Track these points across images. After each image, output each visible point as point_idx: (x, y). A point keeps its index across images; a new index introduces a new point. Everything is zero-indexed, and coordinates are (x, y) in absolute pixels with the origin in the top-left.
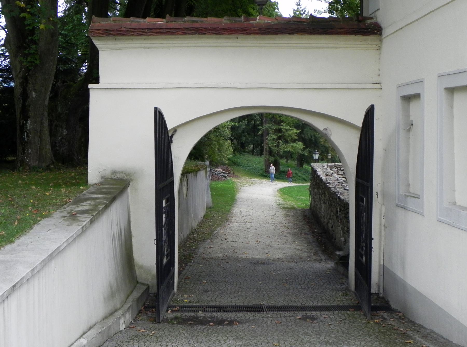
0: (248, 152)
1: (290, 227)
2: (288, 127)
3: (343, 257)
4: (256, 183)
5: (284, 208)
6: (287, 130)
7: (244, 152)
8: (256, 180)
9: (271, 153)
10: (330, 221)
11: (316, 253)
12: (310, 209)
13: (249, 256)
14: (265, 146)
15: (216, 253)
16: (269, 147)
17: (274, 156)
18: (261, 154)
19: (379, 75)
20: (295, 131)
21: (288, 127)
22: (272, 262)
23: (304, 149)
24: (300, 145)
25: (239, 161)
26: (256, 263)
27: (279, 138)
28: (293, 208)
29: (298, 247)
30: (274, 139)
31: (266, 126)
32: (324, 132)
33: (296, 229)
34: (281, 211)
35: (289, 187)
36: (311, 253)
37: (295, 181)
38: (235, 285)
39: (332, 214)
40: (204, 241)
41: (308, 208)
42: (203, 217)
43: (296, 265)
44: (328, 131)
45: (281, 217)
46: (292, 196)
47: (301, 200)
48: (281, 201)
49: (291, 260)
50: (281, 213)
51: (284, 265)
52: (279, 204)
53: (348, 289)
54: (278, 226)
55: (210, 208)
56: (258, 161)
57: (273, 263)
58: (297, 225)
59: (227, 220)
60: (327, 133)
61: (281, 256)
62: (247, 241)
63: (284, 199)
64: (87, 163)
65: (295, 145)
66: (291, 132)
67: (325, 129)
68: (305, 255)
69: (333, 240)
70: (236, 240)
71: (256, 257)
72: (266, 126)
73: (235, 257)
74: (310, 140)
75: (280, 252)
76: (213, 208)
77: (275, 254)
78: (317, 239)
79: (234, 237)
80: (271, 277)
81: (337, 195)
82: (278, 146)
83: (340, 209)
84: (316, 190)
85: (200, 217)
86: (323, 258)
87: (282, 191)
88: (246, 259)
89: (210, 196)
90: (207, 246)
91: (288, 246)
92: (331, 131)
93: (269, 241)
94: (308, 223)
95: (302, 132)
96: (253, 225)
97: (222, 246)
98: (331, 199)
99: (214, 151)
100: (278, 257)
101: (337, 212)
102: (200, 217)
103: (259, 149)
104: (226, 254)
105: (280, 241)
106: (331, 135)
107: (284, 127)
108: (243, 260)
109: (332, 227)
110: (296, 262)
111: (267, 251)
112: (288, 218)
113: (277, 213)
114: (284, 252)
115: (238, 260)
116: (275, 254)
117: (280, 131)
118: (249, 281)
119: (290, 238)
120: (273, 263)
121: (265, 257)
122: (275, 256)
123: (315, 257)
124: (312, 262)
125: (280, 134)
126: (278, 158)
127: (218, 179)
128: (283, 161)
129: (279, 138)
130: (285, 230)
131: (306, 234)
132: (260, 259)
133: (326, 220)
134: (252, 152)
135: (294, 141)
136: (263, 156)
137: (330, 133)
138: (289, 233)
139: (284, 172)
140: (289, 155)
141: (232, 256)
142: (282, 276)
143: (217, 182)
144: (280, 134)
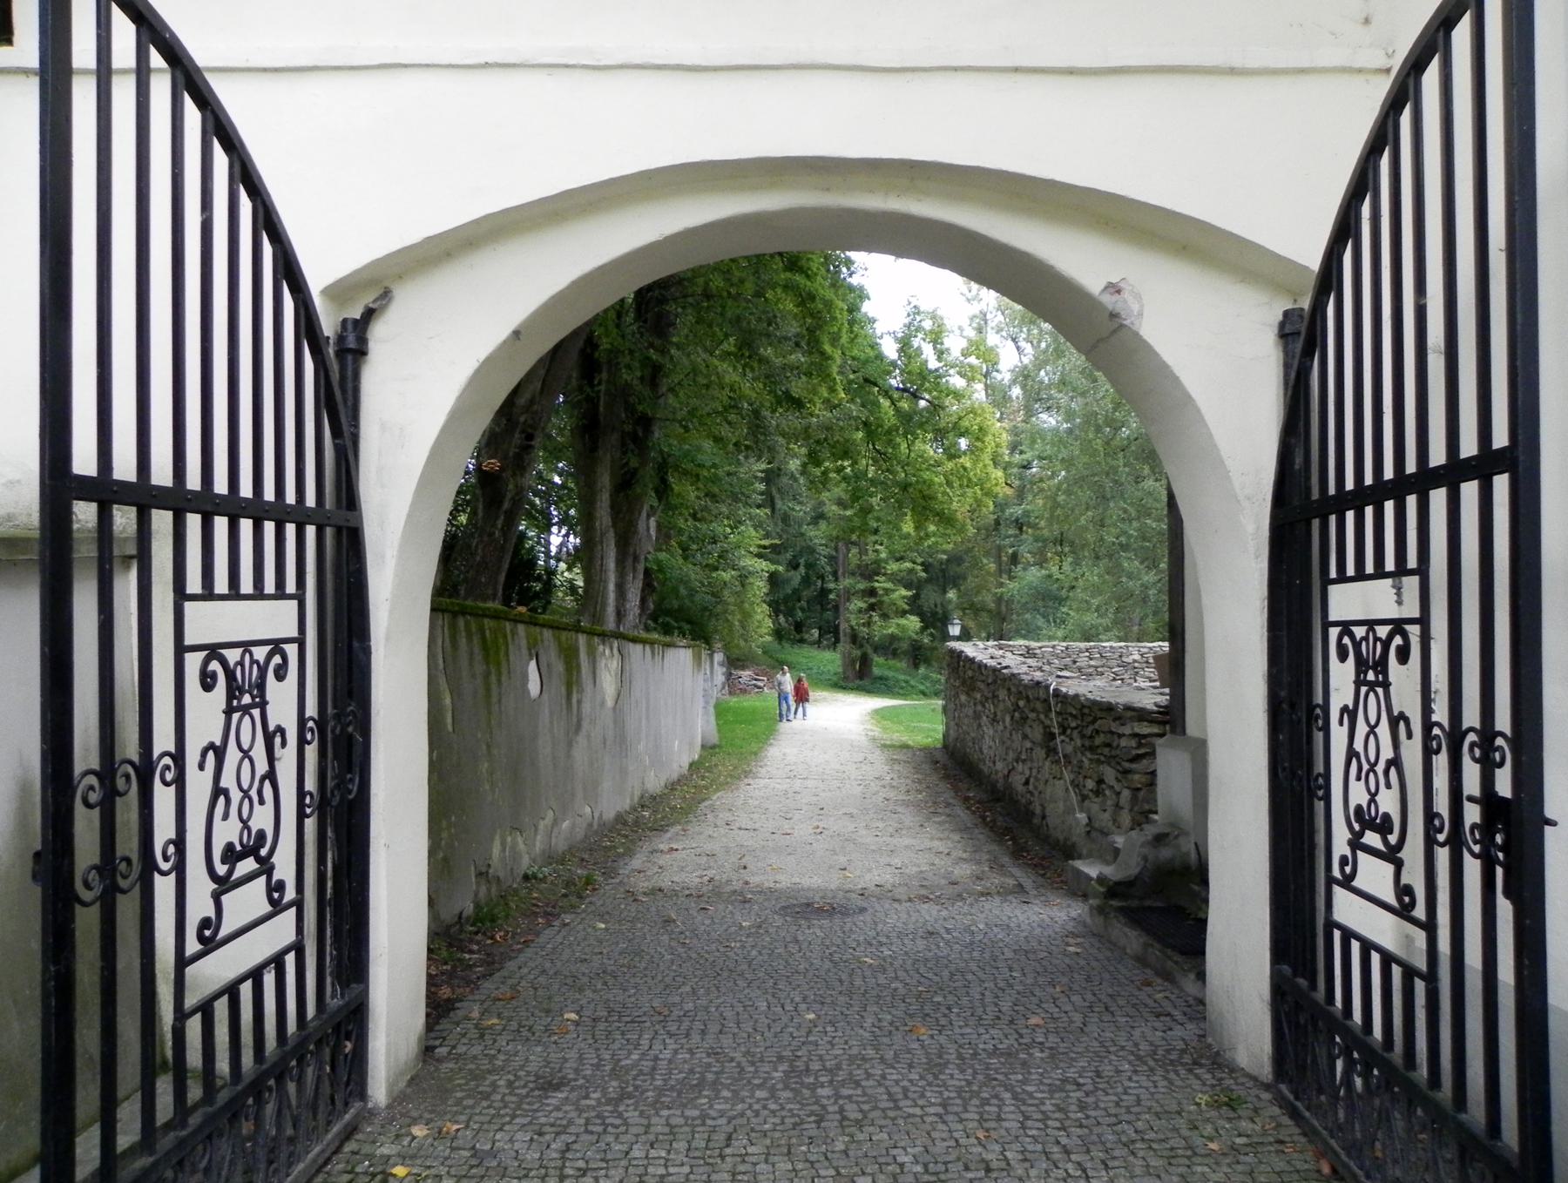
0: (812, 644)
1: (903, 789)
2: (889, 585)
3: (1118, 884)
4: (825, 699)
5: (884, 746)
6: (887, 591)
7: (802, 641)
8: (825, 694)
9: (854, 638)
10: (1020, 767)
11: (995, 865)
12: (945, 746)
13: (785, 881)
14: (843, 626)
15: (682, 869)
16: (852, 628)
17: (861, 646)
18: (834, 646)
19: (1367, 21)
20: (904, 592)
21: (889, 585)
22: (860, 903)
23: (923, 629)
24: (913, 622)
25: (790, 658)
26: (806, 908)
27: (872, 607)
28: (905, 747)
29: (936, 843)
30: (860, 611)
31: (846, 582)
32: (1108, 300)
33: (920, 792)
34: (878, 752)
35: (894, 707)
36: (979, 863)
37: (904, 696)
38: (696, 1038)
39: (1028, 745)
40: (661, 829)
41: (939, 746)
42: (686, 765)
43: (944, 913)
44: (1126, 295)
45: (879, 765)
46: (900, 723)
47: (921, 730)
48: (877, 732)
49: (923, 892)
50: (878, 757)
51: (904, 916)
52: (874, 739)
53: (1210, 1057)
54: (874, 787)
55: (713, 747)
56: (831, 660)
57: (863, 910)
58: (920, 782)
59: (747, 774)
60: (1119, 308)
61: (888, 878)
62: (786, 827)
63: (885, 729)
64: (1203, 953)
65: (903, 621)
66: (895, 596)
67: (1114, 289)
68: (963, 871)
69: (1036, 821)
70: (757, 826)
71: (806, 882)
72: (846, 582)
73: (737, 885)
74: (934, 614)
75: (884, 860)
76: (719, 746)
77: (870, 870)
78: (984, 818)
79: (756, 816)
80: (858, 982)
81: (1048, 687)
82: (868, 624)
83: (1061, 725)
84: (963, 698)
85: (675, 766)
86: (1028, 883)
87: (878, 714)
88: (770, 893)
89: (713, 718)
90: (662, 847)
91: (907, 841)
92: (1138, 297)
93: (851, 828)
94: (946, 777)
95: (916, 597)
96: (810, 783)
97: (708, 847)
98: (1021, 703)
99: (731, 625)
100: (878, 880)
101: (1052, 736)
102: (675, 766)
103: (831, 634)
104: (711, 873)
105: (881, 825)
106: (1141, 314)
107: (881, 584)
108: (761, 898)
109: (1027, 783)
110: (938, 900)
111: (842, 860)
112: (896, 767)
113: (869, 757)
114: (897, 861)
115: (742, 899)
116: (870, 870)
117: (872, 592)
118: (763, 1006)
119: (909, 818)
120: (863, 910)
121: (833, 881)
122: (868, 877)
123: (996, 880)
124: (997, 900)
125: (873, 600)
126: (870, 651)
127: (744, 691)
128: (878, 660)
129: (872, 607)
130: (892, 794)
131: (948, 805)
132: (818, 890)
133: (999, 766)
134: (818, 643)
135: (903, 613)
136: (840, 647)
137: (1135, 307)
138: (906, 804)
139: (881, 678)
140: (889, 647)
141: (729, 881)
142: (901, 974)
143: (742, 698)
144: (873, 600)
